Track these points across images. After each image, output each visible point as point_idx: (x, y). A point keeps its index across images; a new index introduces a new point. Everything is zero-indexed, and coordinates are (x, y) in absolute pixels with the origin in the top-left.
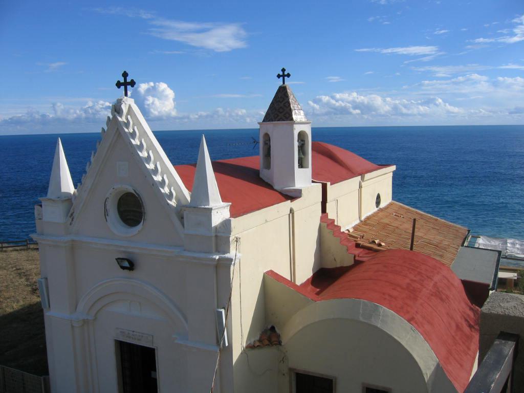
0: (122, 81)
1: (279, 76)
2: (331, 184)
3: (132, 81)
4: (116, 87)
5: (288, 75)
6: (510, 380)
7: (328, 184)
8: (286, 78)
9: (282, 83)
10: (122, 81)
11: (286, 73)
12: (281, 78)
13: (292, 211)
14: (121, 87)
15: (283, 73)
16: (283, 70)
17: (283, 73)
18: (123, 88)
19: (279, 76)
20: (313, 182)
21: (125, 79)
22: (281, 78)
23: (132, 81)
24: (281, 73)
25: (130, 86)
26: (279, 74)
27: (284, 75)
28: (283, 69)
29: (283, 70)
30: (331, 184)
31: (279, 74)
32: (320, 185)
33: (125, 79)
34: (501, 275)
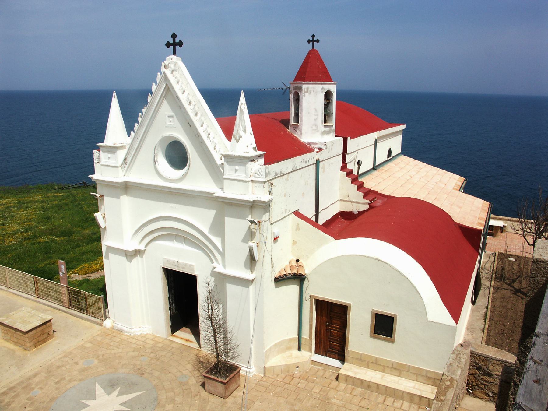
0: (171, 41)
1: (309, 41)
2: (351, 139)
3: (180, 41)
4: (308, 43)
5: (318, 41)
6: (223, 172)
7: (349, 138)
8: (315, 43)
9: (311, 48)
10: (171, 41)
11: (315, 39)
12: (311, 43)
13: (323, 164)
14: (316, 40)
15: (313, 39)
16: (313, 36)
17: (313, 39)
18: (171, 48)
19: (309, 41)
20: (336, 136)
21: (174, 40)
22: (311, 43)
23: (180, 41)
24: (311, 39)
25: (311, 40)
26: (180, 46)
27: (313, 41)
28: (313, 35)
29: (313, 36)
30: (351, 139)
31: (180, 46)
32: (341, 139)
33: (174, 40)
34: (492, 223)
